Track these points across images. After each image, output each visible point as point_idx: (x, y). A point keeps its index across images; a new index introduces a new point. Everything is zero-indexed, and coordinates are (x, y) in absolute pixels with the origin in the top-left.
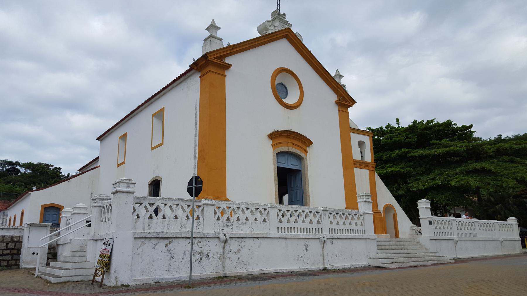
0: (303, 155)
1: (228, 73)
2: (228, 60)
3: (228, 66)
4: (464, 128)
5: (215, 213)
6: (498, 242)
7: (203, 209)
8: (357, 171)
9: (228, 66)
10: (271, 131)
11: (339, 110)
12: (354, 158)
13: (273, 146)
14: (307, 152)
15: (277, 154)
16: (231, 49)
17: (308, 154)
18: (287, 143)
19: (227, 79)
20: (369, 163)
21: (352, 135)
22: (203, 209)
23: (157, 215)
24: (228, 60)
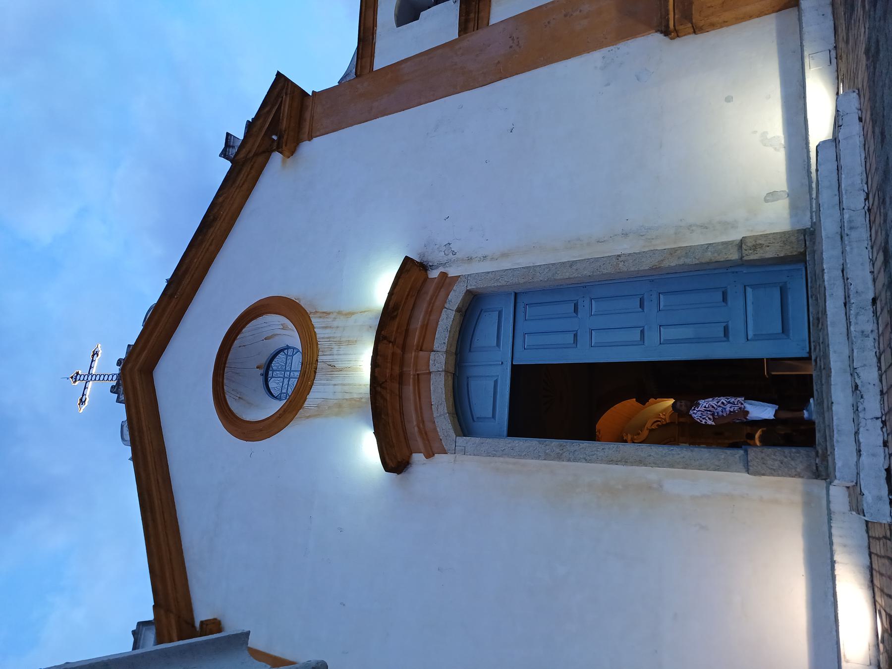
0: (456, 298)
11: (310, 138)
12: (455, 35)
13: (429, 455)
14: (444, 275)
17: (452, 272)
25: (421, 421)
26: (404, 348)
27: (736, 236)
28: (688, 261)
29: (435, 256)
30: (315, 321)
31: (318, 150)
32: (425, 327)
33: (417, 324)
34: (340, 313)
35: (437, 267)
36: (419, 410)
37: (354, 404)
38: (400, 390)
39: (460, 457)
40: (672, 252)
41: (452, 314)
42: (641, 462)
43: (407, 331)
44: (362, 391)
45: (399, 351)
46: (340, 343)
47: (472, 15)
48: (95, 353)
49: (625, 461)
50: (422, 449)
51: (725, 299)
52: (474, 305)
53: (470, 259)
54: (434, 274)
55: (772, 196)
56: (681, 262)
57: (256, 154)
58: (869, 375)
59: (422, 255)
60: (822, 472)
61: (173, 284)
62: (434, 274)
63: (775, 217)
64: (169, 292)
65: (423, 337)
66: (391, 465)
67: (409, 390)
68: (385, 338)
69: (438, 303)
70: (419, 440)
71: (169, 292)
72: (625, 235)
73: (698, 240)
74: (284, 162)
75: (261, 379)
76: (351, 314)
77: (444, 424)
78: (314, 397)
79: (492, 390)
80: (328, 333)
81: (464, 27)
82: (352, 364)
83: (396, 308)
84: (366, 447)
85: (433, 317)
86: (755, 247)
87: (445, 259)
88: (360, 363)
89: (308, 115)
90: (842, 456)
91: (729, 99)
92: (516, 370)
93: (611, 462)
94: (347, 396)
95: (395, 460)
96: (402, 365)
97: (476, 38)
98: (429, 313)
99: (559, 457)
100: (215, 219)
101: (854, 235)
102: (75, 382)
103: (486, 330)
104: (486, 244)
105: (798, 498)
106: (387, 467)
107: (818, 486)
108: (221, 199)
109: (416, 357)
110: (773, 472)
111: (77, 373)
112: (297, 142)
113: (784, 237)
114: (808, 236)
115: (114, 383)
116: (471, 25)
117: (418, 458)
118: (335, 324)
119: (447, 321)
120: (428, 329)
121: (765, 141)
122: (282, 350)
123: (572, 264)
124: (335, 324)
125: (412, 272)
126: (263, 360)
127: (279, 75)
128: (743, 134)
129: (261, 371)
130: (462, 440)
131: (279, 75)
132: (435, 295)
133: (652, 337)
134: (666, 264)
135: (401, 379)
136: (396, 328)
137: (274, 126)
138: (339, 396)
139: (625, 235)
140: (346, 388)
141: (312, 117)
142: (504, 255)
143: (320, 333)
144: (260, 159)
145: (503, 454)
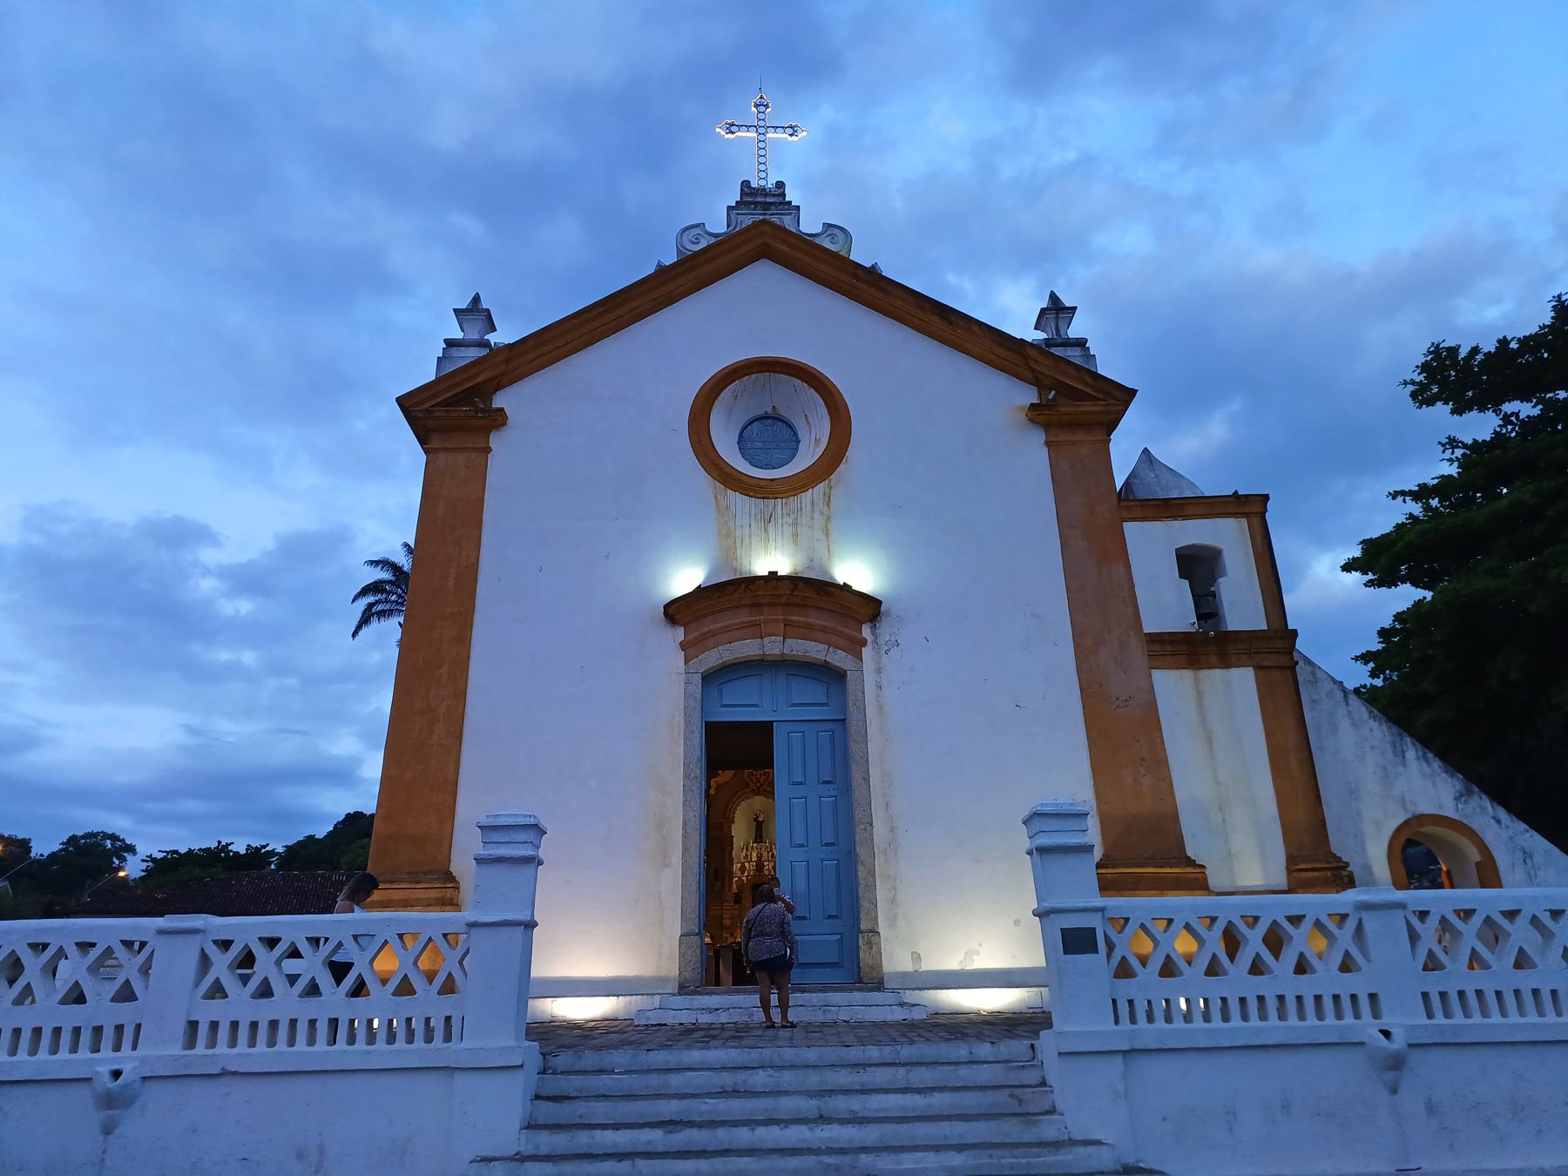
0: (839, 659)
1: (495, 440)
2: (499, 401)
3: (498, 419)
4: (873, 266)
5: (1414, 937)
6: (81, 1094)
7: (1359, 928)
8: (1173, 688)
9: (498, 419)
11: (1048, 444)
12: (1149, 627)
13: (683, 646)
14: (864, 643)
15: (709, 678)
16: (508, 361)
17: (867, 652)
18: (756, 624)
19: (492, 460)
21: (1134, 531)
22: (1359, 928)
23: (1276, 954)
24: (499, 401)
25: (714, 633)
26: (787, 604)
27: (882, 927)
28: (862, 888)
29: (885, 629)
30: (821, 487)
31: (1031, 456)
32: (809, 627)
33: (816, 619)
34: (829, 518)
35: (873, 633)
36: (725, 630)
37: (728, 553)
38: (746, 606)
39: (682, 678)
40: (872, 873)
41: (821, 657)
42: (685, 850)
43: (805, 606)
44: (745, 562)
45: (784, 600)
46: (795, 524)
47: (1169, 648)
48: (793, 130)
49: (685, 836)
50: (691, 637)
51: (830, 917)
52: (834, 677)
53: (879, 671)
54: (866, 632)
55: (917, 957)
56: (862, 882)
57: (1033, 370)
58: (724, 1018)
59: (888, 612)
60: (683, 989)
61: (872, 276)
62: (866, 632)
63: (896, 959)
64: (859, 272)
65: (800, 626)
66: (670, 611)
67: (745, 617)
68: (796, 586)
69: (834, 638)
70: (696, 634)
71: (859, 272)
72: (892, 830)
73: (882, 895)
74: (1021, 409)
75: (761, 412)
76: (827, 535)
77: (712, 658)
78: (737, 500)
79: (747, 704)
80: (807, 507)
81: (1153, 639)
82: (772, 543)
83: (828, 594)
84: (685, 578)
85: (820, 635)
86: (869, 943)
87: (881, 641)
88: (772, 559)
89: (1080, 436)
90: (680, 1001)
91: (1017, 923)
92: (768, 726)
93: (685, 824)
94: (738, 543)
95: (677, 611)
96: (769, 605)
97: (1138, 653)
98: (824, 630)
99: (686, 777)
100: (951, 323)
101: (820, 1013)
102: (756, 106)
103: (808, 691)
104: (894, 692)
105: (663, 973)
106: (668, 606)
107: (796, 975)
108: (976, 329)
109: (777, 621)
110: (682, 955)
111: (767, 106)
112: (1047, 427)
113: (879, 966)
114: (879, 985)
115: (754, 185)
116: (1158, 647)
117: (680, 634)
118: (817, 516)
119: (815, 651)
120: (808, 632)
121: (970, 954)
122: (796, 434)
123: (867, 780)
124: (817, 516)
125: (870, 608)
126: (783, 412)
127: (1133, 392)
128: (969, 940)
129: (770, 411)
130: (697, 679)
131: (1133, 392)
132: (843, 636)
133: (797, 854)
134: (860, 868)
135: (756, 606)
136: (812, 595)
137: (1065, 391)
138: (738, 533)
139: (892, 830)
140: (747, 540)
141: (1075, 443)
142: (880, 709)
143: (806, 496)
144: (1028, 374)
145: (687, 723)
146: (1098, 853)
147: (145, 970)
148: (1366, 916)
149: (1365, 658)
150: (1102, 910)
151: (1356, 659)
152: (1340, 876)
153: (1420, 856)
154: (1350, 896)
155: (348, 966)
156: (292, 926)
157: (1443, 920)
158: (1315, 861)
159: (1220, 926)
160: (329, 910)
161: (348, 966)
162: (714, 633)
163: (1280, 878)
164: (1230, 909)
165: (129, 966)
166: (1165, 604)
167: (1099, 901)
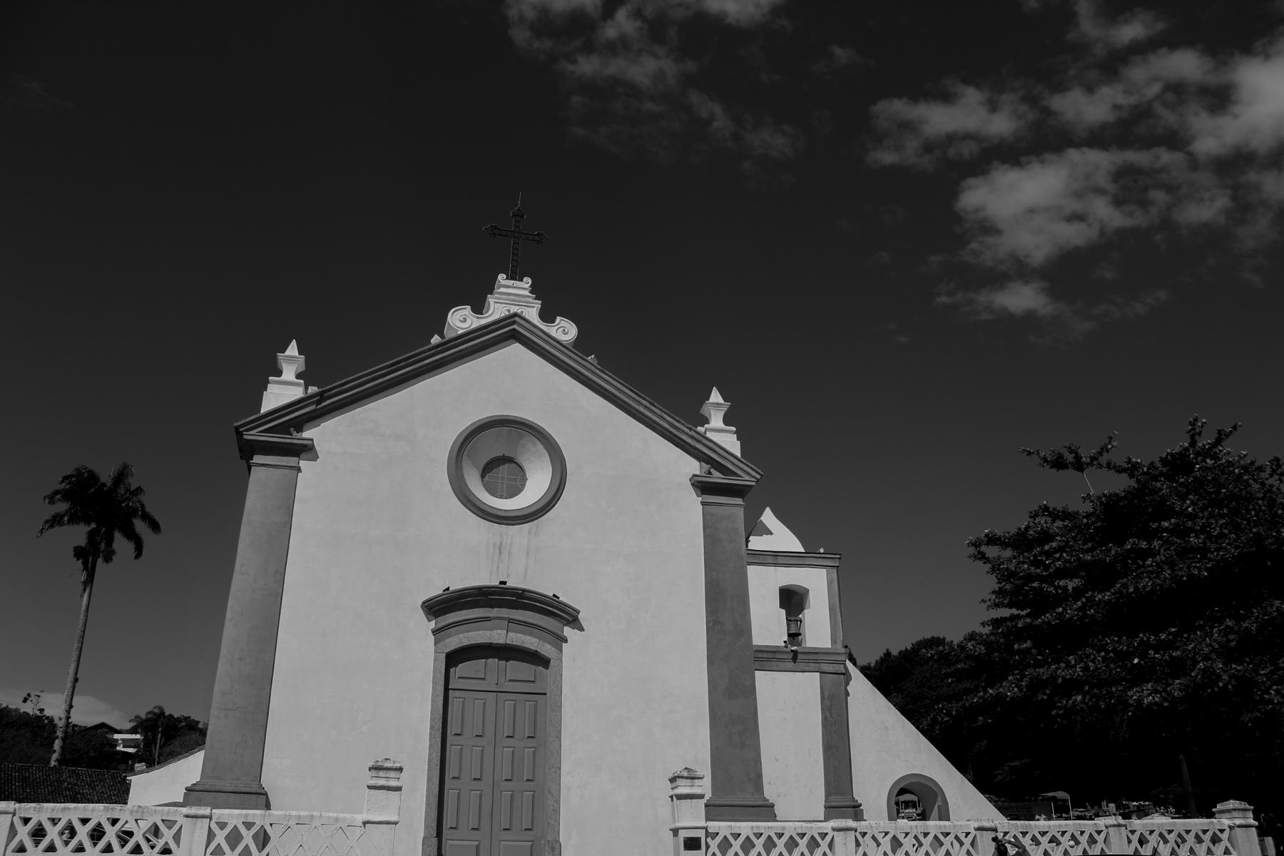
0: (546, 649)
9: (306, 450)
10: (436, 591)
20: (815, 652)
119: (529, 641)
146: (708, 795)
147: (177, 837)
148: (836, 833)
149: (994, 592)
150: (706, 828)
151: (582, 629)
152: (856, 811)
153: (914, 798)
154: (933, 825)
155: (130, 834)
156: (1071, 825)
157: (936, 837)
158: (840, 801)
159: (889, 837)
160: (1033, 819)
161: (130, 834)
162: (487, 619)
163: (821, 814)
164: (790, 829)
165: (167, 836)
166: (768, 626)
167: (703, 824)
